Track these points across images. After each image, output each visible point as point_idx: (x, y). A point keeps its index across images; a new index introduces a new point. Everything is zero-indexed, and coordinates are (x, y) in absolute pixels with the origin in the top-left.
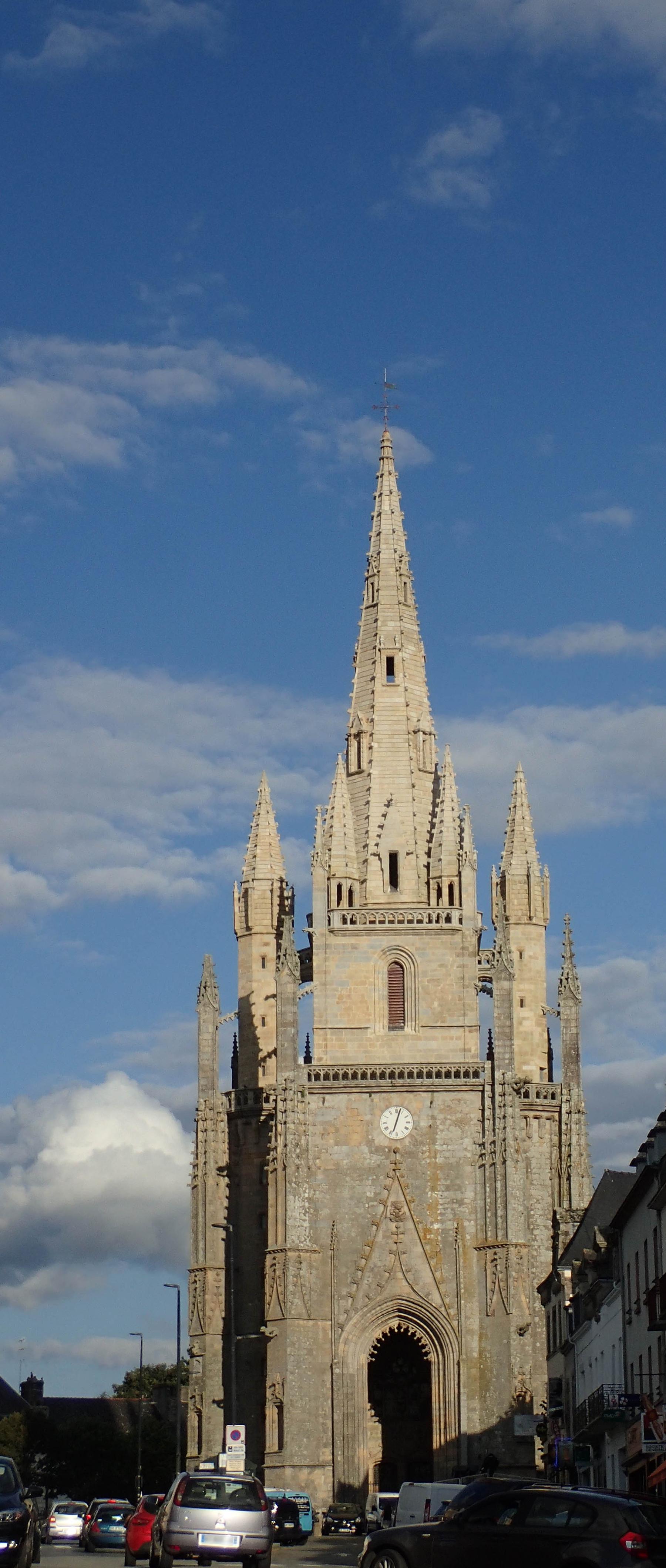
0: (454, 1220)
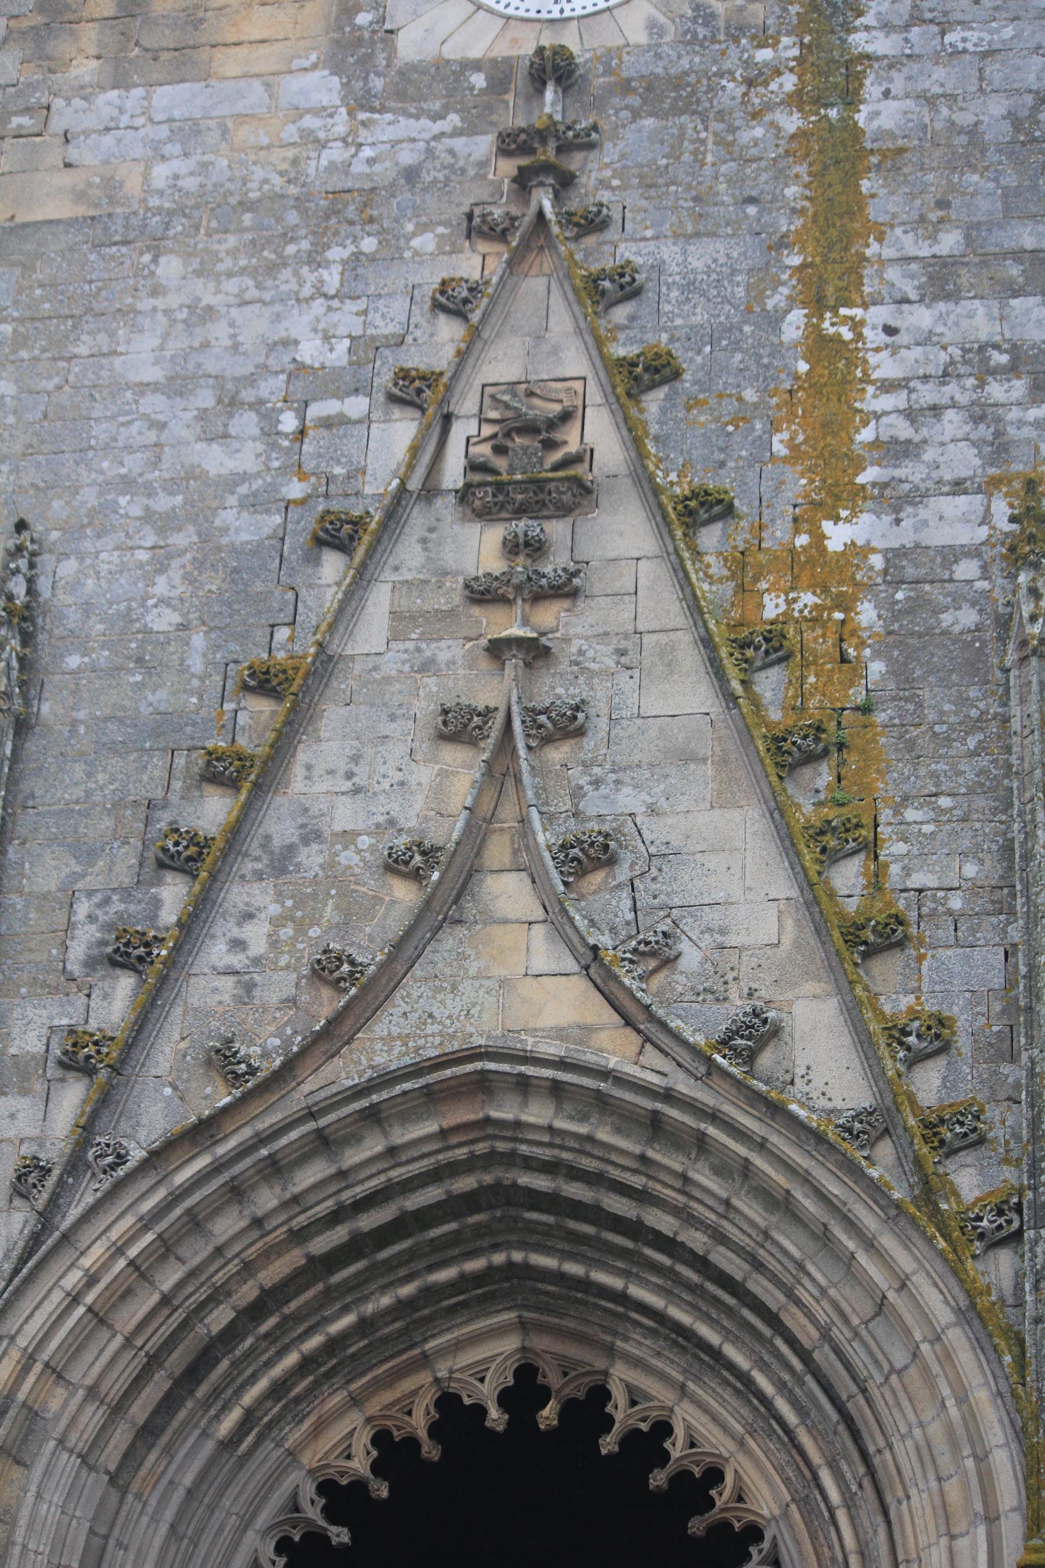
0: (990, 486)
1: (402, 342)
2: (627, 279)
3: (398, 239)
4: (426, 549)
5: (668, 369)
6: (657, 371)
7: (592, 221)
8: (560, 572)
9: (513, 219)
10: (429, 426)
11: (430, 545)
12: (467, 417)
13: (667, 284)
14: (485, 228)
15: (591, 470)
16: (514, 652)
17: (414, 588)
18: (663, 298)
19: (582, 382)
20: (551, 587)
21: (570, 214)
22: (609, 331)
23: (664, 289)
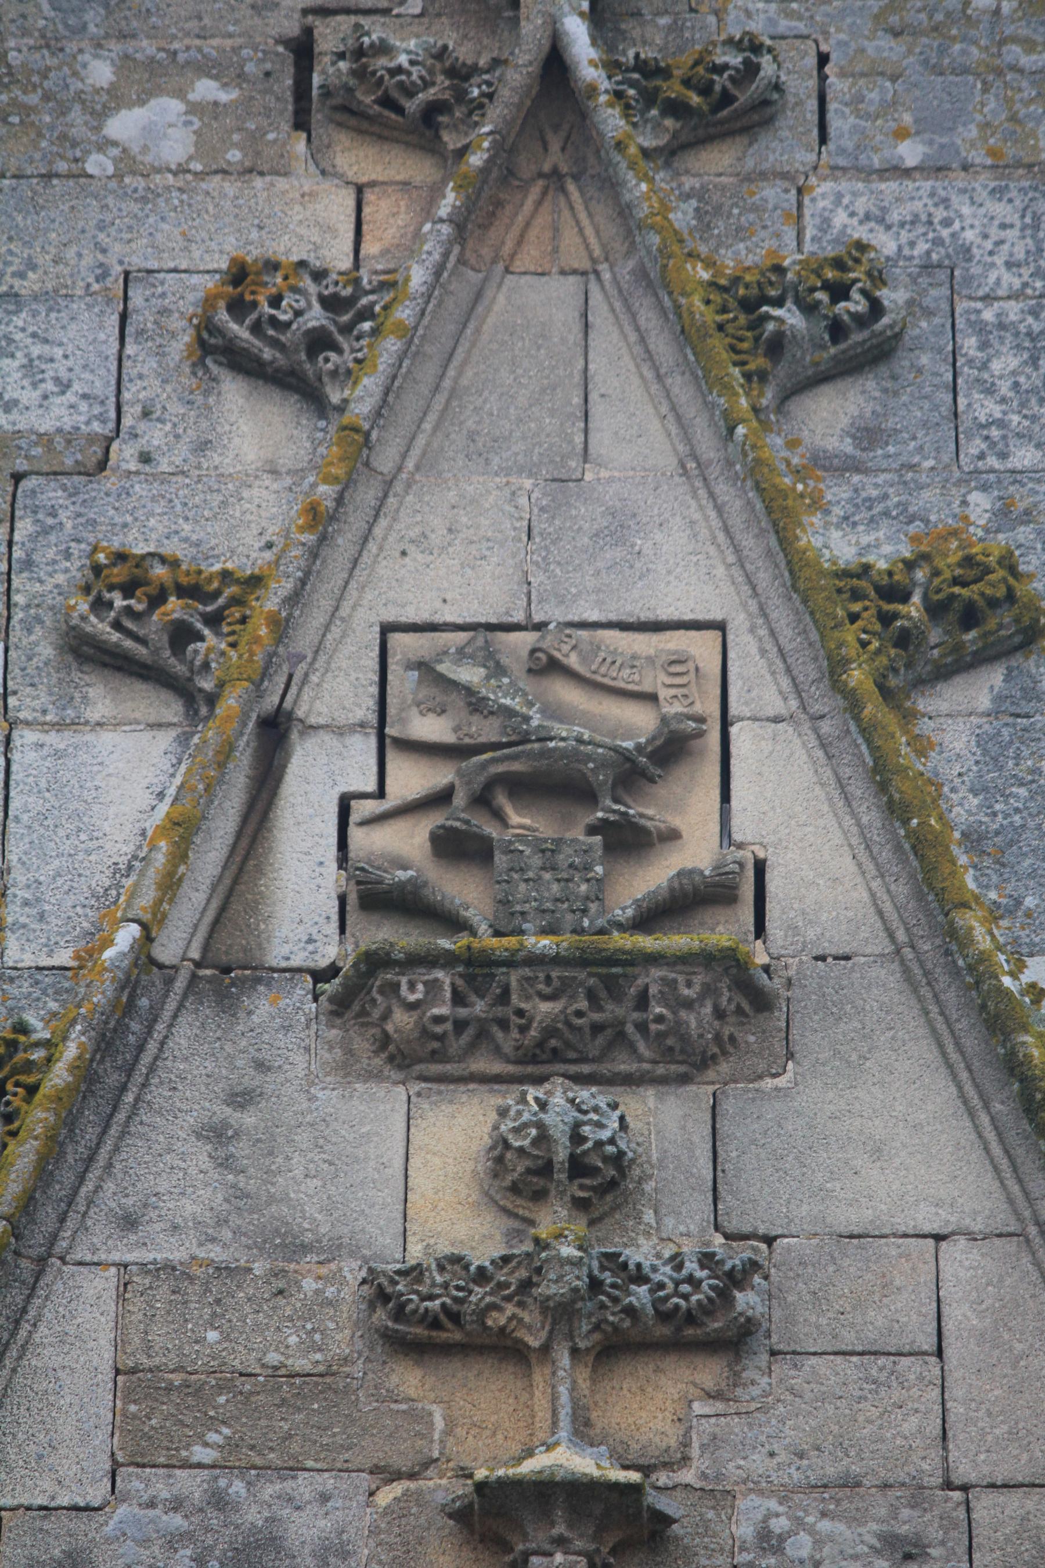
1: (102, 465)
2: (857, 304)
3: (63, 111)
4: (225, 1163)
5: (1006, 616)
6: (970, 617)
7: (727, 99)
8: (691, 1266)
9: (460, 74)
10: (226, 753)
11: (241, 1149)
12: (341, 731)
13: (980, 328)
14: (367, 99)
15: (760, 929)
16: (560, 1529)
17: (194, 1290)
18: (967, 372)
19: (712, 637)
20: (665, 1316)
21: (646, 69)
22: (798, 473)
23: (969, 344)
